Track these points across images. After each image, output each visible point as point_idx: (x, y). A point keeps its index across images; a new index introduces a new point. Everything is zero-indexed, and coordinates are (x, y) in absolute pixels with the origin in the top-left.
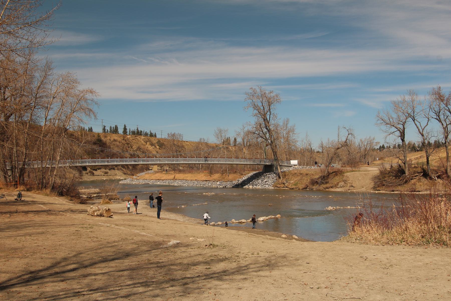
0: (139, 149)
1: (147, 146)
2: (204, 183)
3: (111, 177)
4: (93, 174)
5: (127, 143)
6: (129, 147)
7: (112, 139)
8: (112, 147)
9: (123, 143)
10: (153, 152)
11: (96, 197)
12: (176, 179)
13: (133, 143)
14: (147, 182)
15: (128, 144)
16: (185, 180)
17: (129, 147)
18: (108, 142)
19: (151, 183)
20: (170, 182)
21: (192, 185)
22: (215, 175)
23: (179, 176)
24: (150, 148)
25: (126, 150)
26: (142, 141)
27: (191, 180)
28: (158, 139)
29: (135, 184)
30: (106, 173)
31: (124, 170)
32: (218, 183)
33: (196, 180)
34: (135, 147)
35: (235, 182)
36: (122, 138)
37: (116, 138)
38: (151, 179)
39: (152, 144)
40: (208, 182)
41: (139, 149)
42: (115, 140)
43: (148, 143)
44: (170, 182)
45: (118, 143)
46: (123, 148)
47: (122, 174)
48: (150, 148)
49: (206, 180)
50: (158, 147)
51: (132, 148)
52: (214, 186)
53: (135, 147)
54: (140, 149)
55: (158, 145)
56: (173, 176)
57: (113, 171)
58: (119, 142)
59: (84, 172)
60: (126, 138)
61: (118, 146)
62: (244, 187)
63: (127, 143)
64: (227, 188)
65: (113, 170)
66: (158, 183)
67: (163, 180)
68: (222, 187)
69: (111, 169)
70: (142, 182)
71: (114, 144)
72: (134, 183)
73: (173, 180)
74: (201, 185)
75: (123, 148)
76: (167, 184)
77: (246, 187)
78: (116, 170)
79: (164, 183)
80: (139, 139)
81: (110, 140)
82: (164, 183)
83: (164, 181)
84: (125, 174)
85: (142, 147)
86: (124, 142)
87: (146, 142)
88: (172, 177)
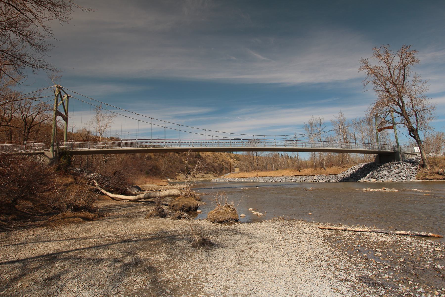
0: (223, 160)
1: (228, 159)
2: (295, 178)
3: (206, 179)
4: (195, 176)
5: (216, 157)
6: (217, 160)
7: (207, 155)
8: (206, 160)
9: (213, 157)
10: (232, 163)
11: (145, 198)
12: (259, 177)
13: (219, 157)
14: (232, 180)
15: (216, 158)
16: (270, 176)
17: (217, 160)
18: (204, 156)
19: (236, 180)
20: (254, 179)
21: (280, 181)
22: (304, 170)
23: (260, 174)
24: (230, 160)
25: (215, 162)
26: (225, 156)
27: (277, 176)
28: (235, 155)
29: (222, 182)
30: (203, 176)
31: (214, 174)
32: (315, 177)
33: (283, 176)
34: (221, 160)
35: (341, 176)
36: (213, 154)
37: (209, 154)
38: (236, 177)
39: (231, 158)
40: (301, 177)
41: (223, 160)
42: (208, 155)
43: (229, 157)
44: (254, 179)
45: (210, 157)
46: (214, 160)
47: (213, 176)
48: (230, 160)
49: (297, 175)
50: (235, 159)
51: (219, 160)
52: (310, 181)
53: (221, 160)
54: (224, 161)
55: (235, 159)
56: (256, 174)
57: (207, 174)
58: (211, 157)
59: (189, 175)
60: (215, 154)
61: (210, 159)
62: (361, 180)
63: (216, 157)
64: (330, 182)
65: (208, 174)
66: (243, 180)
67: (247, 178)
68: (324, 181)
69: (206, 173)
70: (228, 180)
71: (208, 158)
72: (222, 181)
73: (257, 178)
74: (293, 181)
75: (214, 160)
76: (251, 181)
77: (364, 180)
78: (209, 174)
79: (248, 180)
80: (223, 155)
81: (205, 155)
82: (248, 180)
83: (248, 179)
84: (215, 176)
85: (225, 159)
86: (214, 156)
87: (228, 157)
88: (255, 174)
